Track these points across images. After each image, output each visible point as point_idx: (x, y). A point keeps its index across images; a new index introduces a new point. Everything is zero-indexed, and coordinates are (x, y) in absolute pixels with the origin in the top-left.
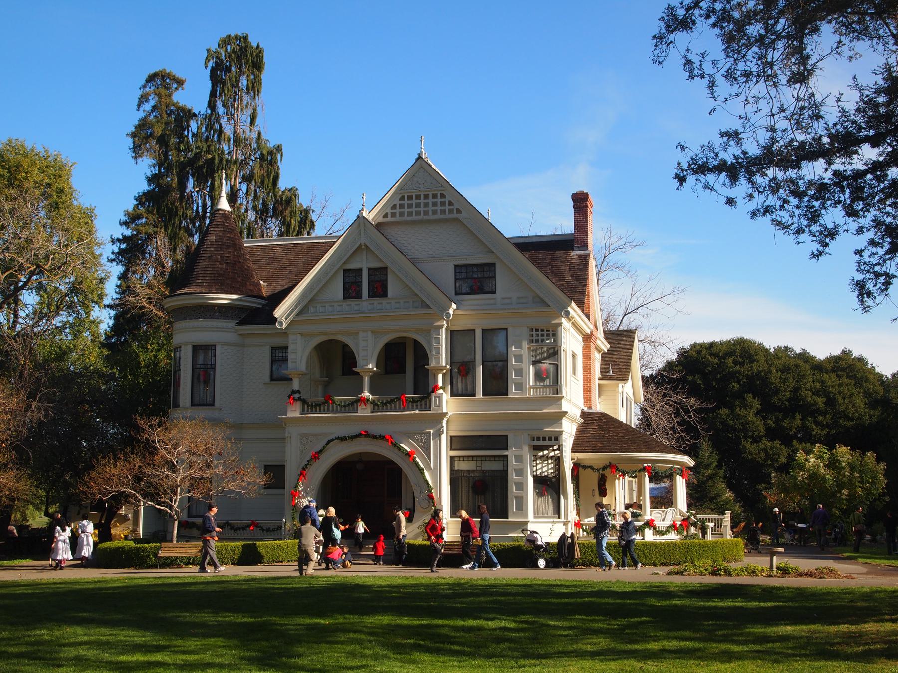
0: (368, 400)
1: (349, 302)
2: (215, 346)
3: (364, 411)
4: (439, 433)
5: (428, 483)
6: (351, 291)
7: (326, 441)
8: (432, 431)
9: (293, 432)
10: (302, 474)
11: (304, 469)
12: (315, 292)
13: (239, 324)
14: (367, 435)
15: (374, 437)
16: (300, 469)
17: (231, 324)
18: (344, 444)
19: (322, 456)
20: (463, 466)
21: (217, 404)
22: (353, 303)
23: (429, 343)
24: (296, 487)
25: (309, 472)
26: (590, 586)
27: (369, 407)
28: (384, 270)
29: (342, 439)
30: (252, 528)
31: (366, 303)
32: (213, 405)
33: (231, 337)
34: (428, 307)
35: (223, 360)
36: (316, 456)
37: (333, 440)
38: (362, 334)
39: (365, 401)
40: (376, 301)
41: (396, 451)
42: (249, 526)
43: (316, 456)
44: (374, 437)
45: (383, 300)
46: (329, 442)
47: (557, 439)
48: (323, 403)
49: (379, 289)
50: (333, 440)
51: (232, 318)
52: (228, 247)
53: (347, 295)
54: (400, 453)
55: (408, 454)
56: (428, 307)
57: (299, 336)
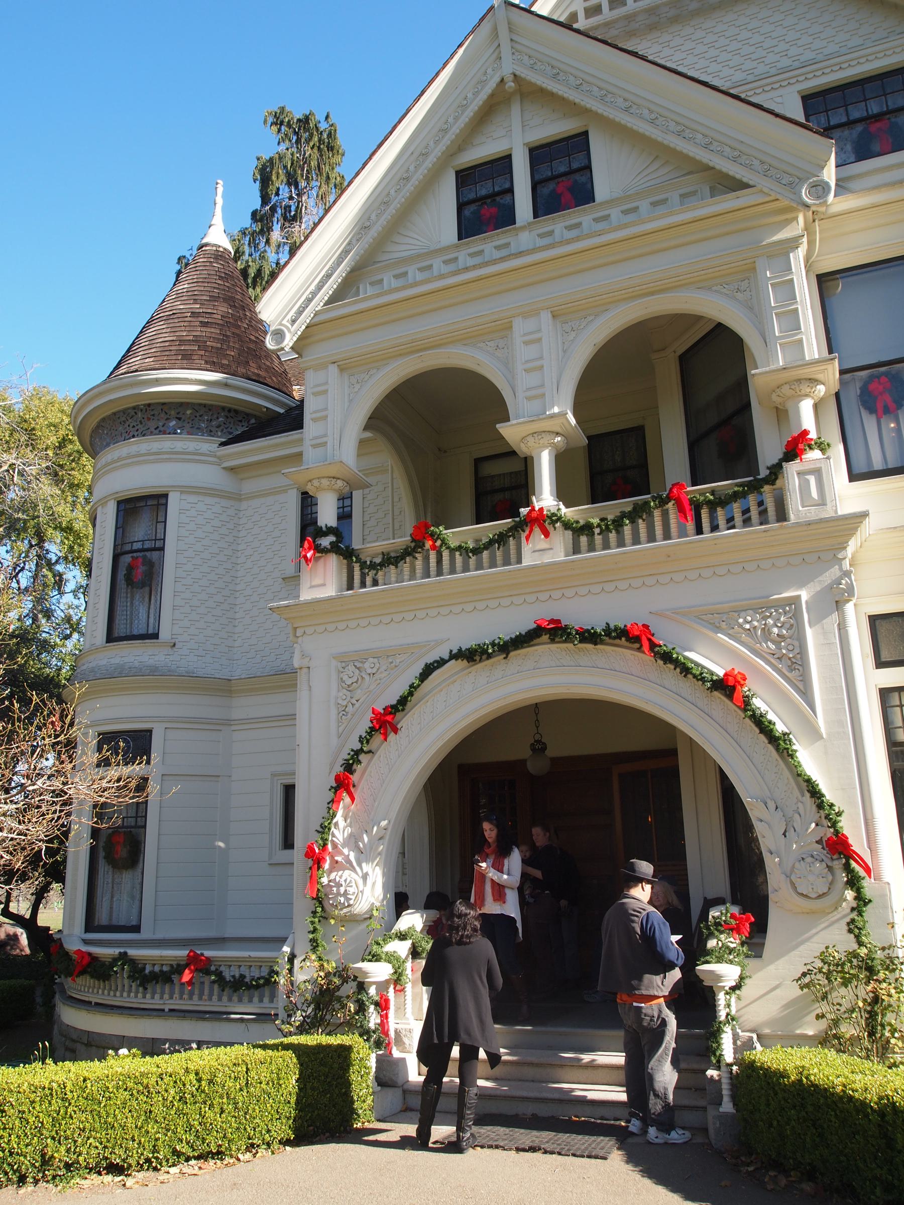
0: (555, 518)
1: (477, 243)
2: (166, 496)
3: (542, 552)
4: (836, 599)
5: (815, 793)
6: (482, 203)
7: (418, 668)
8: (805, 595)
9: (317, 653)
10: (343, 784)
11: (349, 768)
12: (373, 233)
13: (223, 444)
14: (555, 631)
15: (589, 637)
16: (338, 769)
17: (207, 445)
18: (481, 671)
19: (407, 722)
21: (164, 634)
22: (488, 244)
23: (756, 310)
24: (324, 829)
25: (366, 777)
26: (397, 872)
27: (560, 540)
28: (578, 143)
29: (472, 655)
30: (187, 976)
31: (527, 231)
32: (155, 636)
33: (208, 474)
34: (740, 186)
35: (185, 535)
36: (385, 722)
37: (441, 663)
38: (520, 327)
39: (543, 522)
40: (558, 224)
41: (670, 674)
42: (178, 969)
43: (385, 722)
44: (589, 637)
45: (583, 216)
46: (428, 671)
47: (294, 774)
48: (414, 550)
49: (564, 176)
50: (441, 663)
51: (210, 433)
52: (213, 299)
53: (468, 228)
54: (687, 686)
55: (726, 687)
56: (740, 186)
57: (333, 369)
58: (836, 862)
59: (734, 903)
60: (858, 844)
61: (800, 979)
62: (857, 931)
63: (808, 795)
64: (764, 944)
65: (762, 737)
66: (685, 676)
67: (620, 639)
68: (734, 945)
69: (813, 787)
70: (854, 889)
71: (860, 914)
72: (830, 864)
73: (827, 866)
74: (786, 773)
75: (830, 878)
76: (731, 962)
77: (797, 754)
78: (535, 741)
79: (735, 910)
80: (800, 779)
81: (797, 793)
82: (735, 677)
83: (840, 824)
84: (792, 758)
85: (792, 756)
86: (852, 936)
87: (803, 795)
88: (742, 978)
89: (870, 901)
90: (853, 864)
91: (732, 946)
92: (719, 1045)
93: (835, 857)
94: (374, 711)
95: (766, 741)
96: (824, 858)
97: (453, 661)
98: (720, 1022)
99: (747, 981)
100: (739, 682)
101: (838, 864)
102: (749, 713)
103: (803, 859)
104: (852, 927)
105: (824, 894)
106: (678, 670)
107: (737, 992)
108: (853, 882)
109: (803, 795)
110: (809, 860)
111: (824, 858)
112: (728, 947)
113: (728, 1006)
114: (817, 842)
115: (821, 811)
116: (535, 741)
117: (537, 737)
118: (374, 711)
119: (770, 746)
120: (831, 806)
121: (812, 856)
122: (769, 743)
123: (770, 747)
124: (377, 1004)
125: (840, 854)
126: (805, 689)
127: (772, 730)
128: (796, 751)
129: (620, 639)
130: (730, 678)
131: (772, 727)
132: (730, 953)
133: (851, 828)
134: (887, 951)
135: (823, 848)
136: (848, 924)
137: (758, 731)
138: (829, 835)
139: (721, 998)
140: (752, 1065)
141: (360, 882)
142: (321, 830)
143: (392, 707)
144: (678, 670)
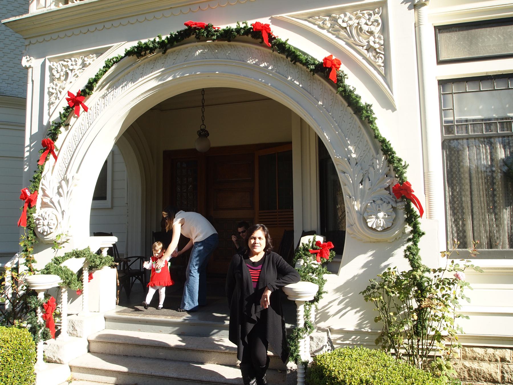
20: (476, 107)
55: (325, 70)
58: (399, 204)
59: (322, 234)
60: (418, 191)
61: (365, 292)
62: (411, 256)
63: (381, 153)
64: (340, 262)
65: (350, 109)
66: (294, 63)
67: (247, 35)
68: (317, 266)
69: (386, 146)
70: (412, 224)
71: (415, 244)
72: (394, 205)
73: (392, 207)
74: (367, 137)
75: (394, 216)
76: (312, 280)
77: (376, 121)
78: (201, 130)
79: (320, 239)
80: (377, 140)
81: (373, 151)
82: (332, 61)
83: (405, 175)
84: (372, 124)
85: (371, 122)
86: (407, 259)
87: (377, 153)
88: (319, 293)
89: (423, 234)
90: (413, 206)
91: (315, 267)
92: (297, 347)
93: (399, 200)
94: (69, 94)
95: (352, 112)
96: (390, 200)
97: (127, 57)
98: (299, 330)
99: (323, 295)
100: (335, 65)
101: (401, 206)
102: (341, 89)
103: (374, 201)
104: (408, 253)
105: (388, 228)
106: (289, 59)
107: (316, 303)
108: (411, 219)
109: (377, 153)
110: (379, 202)
111: (390, 200)
112: (312, 268)
113: (307, 316)
114: (386, 189)
115: (391, 165)
116: (201, 130)
117: (203, 127)
118: (69, 94)
119: (355, 116)
120: (400, 160)
121: (381, 199)
122: (355, 113)
123: (355, 116)
124: (42, 307)
125: (403, 198)
126: (385, 73)
127: (357, 102)
128: (375, 118)
129: (247, 35)
130: (328, 62)
131: (358, 99)
132: (313, 273)
133: (413, 177)
134: (437, 273)
135: (390, 194)
136: (405, 251)
137: (346, 105)
138: (395, 183)
139: (301, 310)
140: (322, 370)
141: (60, 216)
142: (33, 180)
143: (84, 91)
144: (289, 59)
